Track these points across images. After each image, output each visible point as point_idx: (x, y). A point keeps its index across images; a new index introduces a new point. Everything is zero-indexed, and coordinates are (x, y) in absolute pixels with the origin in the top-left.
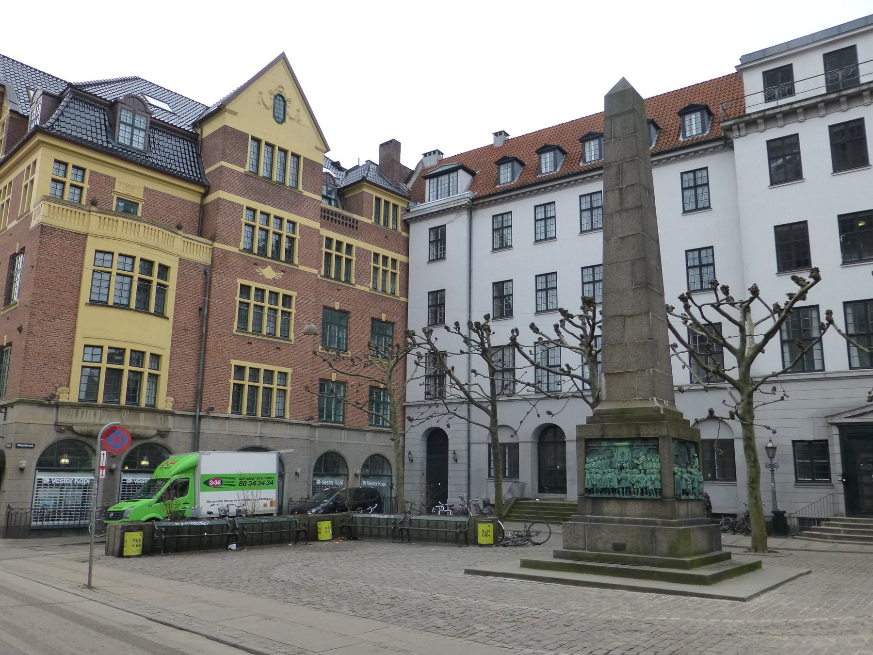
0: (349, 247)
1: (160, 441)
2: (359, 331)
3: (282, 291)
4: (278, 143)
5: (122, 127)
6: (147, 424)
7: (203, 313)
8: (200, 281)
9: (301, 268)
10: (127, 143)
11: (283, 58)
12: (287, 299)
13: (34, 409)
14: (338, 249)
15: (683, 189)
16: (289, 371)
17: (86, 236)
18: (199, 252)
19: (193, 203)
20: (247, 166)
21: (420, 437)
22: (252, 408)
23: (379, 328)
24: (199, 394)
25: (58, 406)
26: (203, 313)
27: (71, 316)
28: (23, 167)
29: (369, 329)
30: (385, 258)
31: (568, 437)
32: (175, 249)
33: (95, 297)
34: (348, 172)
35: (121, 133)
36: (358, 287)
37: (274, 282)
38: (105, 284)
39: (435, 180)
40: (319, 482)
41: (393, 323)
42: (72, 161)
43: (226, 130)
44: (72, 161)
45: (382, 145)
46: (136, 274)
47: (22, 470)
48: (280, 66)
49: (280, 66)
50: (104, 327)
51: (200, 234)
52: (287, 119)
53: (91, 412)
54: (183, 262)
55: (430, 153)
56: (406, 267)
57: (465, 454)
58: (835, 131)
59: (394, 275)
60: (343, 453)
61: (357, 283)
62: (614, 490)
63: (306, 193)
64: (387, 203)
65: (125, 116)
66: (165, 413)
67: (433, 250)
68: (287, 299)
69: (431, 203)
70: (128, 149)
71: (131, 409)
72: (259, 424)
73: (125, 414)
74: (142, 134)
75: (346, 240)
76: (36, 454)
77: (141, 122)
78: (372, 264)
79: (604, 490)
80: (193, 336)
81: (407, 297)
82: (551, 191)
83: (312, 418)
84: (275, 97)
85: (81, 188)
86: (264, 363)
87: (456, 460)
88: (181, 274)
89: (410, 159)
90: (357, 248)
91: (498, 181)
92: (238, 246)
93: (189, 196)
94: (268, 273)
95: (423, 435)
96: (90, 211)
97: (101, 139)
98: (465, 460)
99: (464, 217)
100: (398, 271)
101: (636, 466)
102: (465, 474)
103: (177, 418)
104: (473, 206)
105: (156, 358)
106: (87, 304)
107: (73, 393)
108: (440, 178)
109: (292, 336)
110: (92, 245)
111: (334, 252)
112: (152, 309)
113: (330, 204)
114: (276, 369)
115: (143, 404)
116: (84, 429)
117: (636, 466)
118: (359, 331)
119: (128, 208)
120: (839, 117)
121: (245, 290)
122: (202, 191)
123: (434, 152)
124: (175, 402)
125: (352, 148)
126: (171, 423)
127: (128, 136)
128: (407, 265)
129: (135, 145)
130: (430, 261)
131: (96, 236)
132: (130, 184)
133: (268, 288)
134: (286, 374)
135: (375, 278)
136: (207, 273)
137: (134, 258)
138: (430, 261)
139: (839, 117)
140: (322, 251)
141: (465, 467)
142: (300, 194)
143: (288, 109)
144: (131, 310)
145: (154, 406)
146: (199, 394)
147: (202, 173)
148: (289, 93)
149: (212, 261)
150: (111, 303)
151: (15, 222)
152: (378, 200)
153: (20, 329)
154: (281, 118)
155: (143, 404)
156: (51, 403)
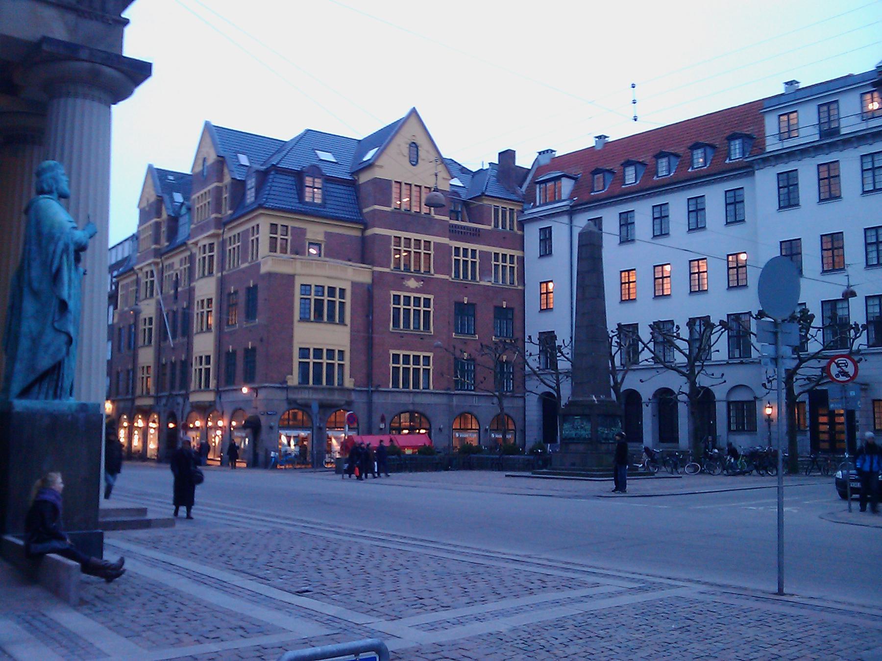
0: (474, 251)
2: (485, 316)
5: (307, 189)
9: (437, 276)
10: (316, 180)
11: (414, 112)
12: (427, 302)
14: (465, 255)
15: (727, 204)
16: (431, 355)
18: (362, 274)
22: (416, 385)
28: (249, 226)
29: (492, 315)
30: (504, 256)
31: (644, 399)
32: (348, 275)
35: (307, 194)
36: (482, 283)
37: (416, 290)
38: (307, 306)
41: (512, 309)
42: (280, 222)
43: (377, 182)
44: (280, 222)
48: (413, 120)
49: (413, 120)
50: (308, 335)
53: (307, 391)
54: (354, 285)
55: (544, 152)
56: (522, 260)
59: (512, 268)
62: (574, 439)
63: (437, 217)
65: (308, 181)
68: (427, 302)
70: (313, 204)
72: (411, 395)
77: (318, 183)
79: (570, 439)
83: (449, 389)
84: (410, 146)
88: (353, 293)
89: (525, 160)
93: (352, 232)
94: (412, 283)
97: (294, 204)
99: (565, 219)
100: (515, 265)
101: (582, 428)
104: (571, 212)
105: (341, 353)
107: (294, 380)
114: (422, 354)
116: (303, 402)
117: (582, 428)
118: (485, 316)
125: (478, 156)
130: (541, 256)
131: (300, 275)
132: (316, 231)
133: (412, 295)
134: (429, 357)
135: (496, 273)
143: (420, 153)
146: (369, 376)
147: (361, 213)
148: (421, 140)
151: (246, 265)
153: (261, 340)
154: (414, 161)
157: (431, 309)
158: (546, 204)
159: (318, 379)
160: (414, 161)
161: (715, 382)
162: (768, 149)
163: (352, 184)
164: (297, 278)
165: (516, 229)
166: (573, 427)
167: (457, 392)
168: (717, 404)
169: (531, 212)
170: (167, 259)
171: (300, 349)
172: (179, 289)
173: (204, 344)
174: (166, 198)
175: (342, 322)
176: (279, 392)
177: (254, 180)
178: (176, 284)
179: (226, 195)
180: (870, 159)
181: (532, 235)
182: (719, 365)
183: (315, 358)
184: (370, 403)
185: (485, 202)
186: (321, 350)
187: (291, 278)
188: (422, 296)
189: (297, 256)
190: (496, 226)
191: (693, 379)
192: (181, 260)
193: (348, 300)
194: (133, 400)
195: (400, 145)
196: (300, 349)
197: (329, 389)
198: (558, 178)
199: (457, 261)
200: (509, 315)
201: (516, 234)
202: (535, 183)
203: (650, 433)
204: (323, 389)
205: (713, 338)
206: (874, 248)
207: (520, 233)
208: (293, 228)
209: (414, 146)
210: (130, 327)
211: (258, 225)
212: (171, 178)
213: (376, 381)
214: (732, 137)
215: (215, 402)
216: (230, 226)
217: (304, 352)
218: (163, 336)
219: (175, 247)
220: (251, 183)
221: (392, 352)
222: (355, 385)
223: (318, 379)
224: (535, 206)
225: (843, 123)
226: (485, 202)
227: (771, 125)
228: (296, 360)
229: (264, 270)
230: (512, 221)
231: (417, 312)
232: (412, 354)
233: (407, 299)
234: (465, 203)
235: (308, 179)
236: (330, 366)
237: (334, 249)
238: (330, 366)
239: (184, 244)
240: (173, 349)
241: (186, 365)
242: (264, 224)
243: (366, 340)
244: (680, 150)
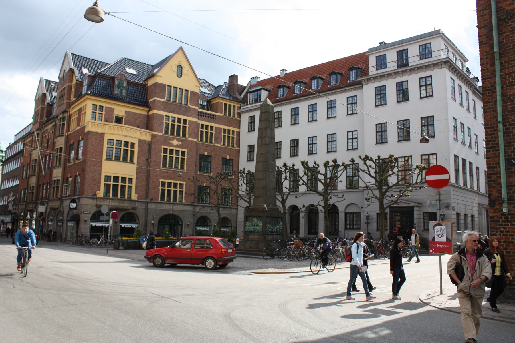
0: (212, 127)
1: (133, 211)
6: (128, 205)
8: (147, 147)
12: (183, 153)
13: (188, 206)
14: (207, 129)
18: (146, 136)
20: (166, 98)
22: (169, 199)
23: (226, 162)
24: (147, 194)
25: (97, 198)
29: (221, 163)
32: (136, 135)
33: (108, 157)
34: (216, 88)
37: (177, 146)
40: (198, 228)
41: (232, 160)
43: (156, 84)
45: (230, 77)
46: (122, 148)
47: (86, 221)
48: (180, 52)
49: (180, 52)
50: (111, 168)
51: (147, 129)
52: (183, 75)
54: (140, 141)
56: (239, 134)
58: (399, 85)
60: (209, 216)
61: (215, 143)
62: (252, 232)
63: (191, 107)
66: (135, 201)
68: (183, 153)
71: (122, 200)
75: (210, 124)
76: (90, 216)
78: (223, 134)
79: (250, 232)
81: (239, 147)
82: (297, 102)
83: (194, 202)
84: (178, 67)
85: (102, 114)
88: (139, 146)
89: (243, 81)
90: (216, 127)
92: (162, 132)
94: (175, 142)
100: (235, 136)
103: (139, 203)
105: (130, 180)
107: (101, 193)
109: (185, 168)
111: (205, 130)
112: (129, 161)
115: (126, 197)
117: (257, 225)
119: (119, 120)
120: (399, 79)
121: (165, 150)
122: (148, 109)
123: (255, 77)
126: (137, 205)
128: (240, 133)
133: (175, 149)
135: (224, 140)
137: (121, 141)
138: (249, 131)
139: (399, 79)
140: (198, 131)
143: (183, 71)
145: (130, 198)
146: (147, 194)
148: (184, 64)
154: (180, 74)
155: (126, 197)
157: (186, 157)
158: (253, 103)
159: (115, 193)
160: (180, 74)
161: (339, 199)
162: (370, 74)
164: (105, 135)
165: (236, 116)
166: (252, 224)
167: (199, 204)
168: (340, 214)
169: (244, 108)
171: (105, 176)
175: (132, 161)
176: (91, 200)
177: (87, 80)
178: (48, 141)
179: (73, 90)
180: (424, 80)
181: (245, 120)
182: (342, 192)
184: (147, 209)
186: (118, 177)
187: (102, 135)
188: (181, 150)
189: (107, 123)
190: (225, 114)
191: (326, 196)
193: (136, 150)
195: (172, 65)
196: (105, 176)
197: (122, 200)
198: (260, 90)
199: (202, 132)
200: (230, 163)
201: (236, 119)
202: (247, 93)
203: (303, 230)
204: (118, 199)
205: (338, 174)
206: (424, 88)
207: (238, 119)
208: (106, 107)
209: (180, 67)
210: (28, 164)
211: (86, 105)
212: (53, 84)
213: (150, 197)
214: (352, 69)
217: (108, 178)
220: (86, 82)
221: (161, 180)
222: (138, 198)
223: (115, 193)
224: (247, 105)
225: (410, 60)
227: (372, 61)
228: (103, 182)
229: (86, 131)
230: (234, 112)
231: (177, 159)
232: (167, 181)
233: (171, 151)
234: (209, 102)
236: (123, 187)
237: (131, 121)
238: (123, 187)
243: (145, 174)
244: (324, 76)
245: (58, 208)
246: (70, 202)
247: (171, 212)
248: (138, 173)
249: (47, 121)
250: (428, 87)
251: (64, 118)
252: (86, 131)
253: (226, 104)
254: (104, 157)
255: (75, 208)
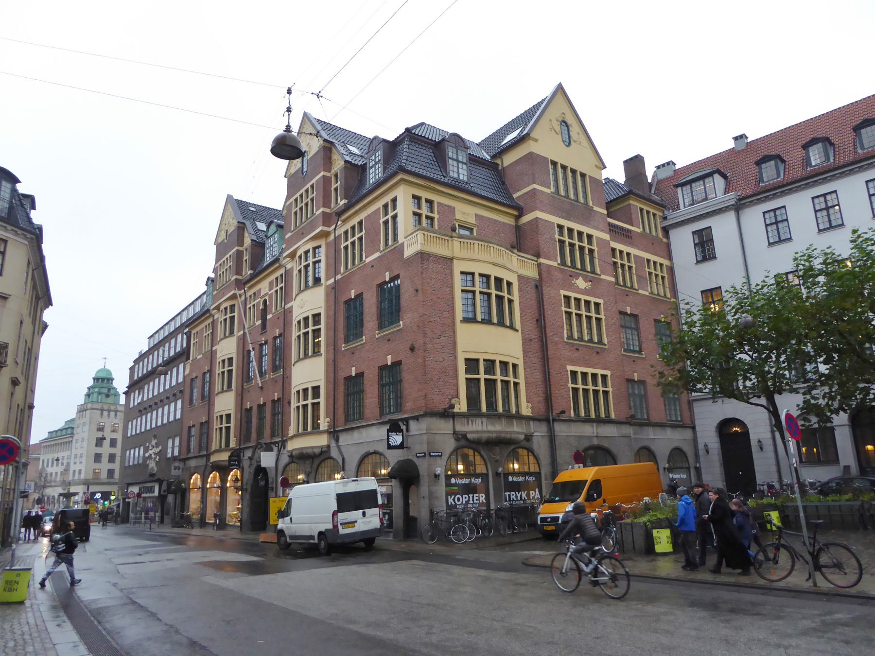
3: (593, 300)
4: (570, 165)
7: (541, 322)
8: (532, 294)
10: (456, 176)
11: (560, 89)
12: (597, 305)
17: (451, 259)
19: (510, 225)
21: (714, 429)
24: (548, 399)
26: (541, 322)
27: (451, 333)
28: (379, 204)
32: (515, 268)
37: (585, 292)
39: (688, 187)
42: (424, 195)
48: (559, 96)
49: (559, 96)
54: (520, 278)
55: (663, 165)
56: (671, 270)
57: (771, 442)
63: (595, 208)
64: (648, 212)
67: (699, 250)
69: (685, 210)
70: (457, 180)
73: (504, 421)
74: (465, 167)
80: (536, 345)
86: (590, 367)
87: (761, 448)
91: (761, 180)
94: (581, 283)
95: (717, 427)
96: (452, 237)
98: (772, 448)
99: (731, 216)
102: (773, 461)
104: (738, 207)
106: (461, 321)
107: (462, 406)
108: (693, 185)
109: (605, 341)
110: (458, 267)
113: (319, 261)
115: (484, 409)
122: (516, 213)
123: (668, 163)
124: (532, 408)
127: (455, 169)
129: (461, 177)
130: (698, 262)
132: (466, 212)
136: (538, 287)
138: (698, 262)
141: (772, 455)
142: (591, 209)
144: (494, 324)
146: (548, 399)
147: (511, 197)
148: (570, 120)
149: (540, 274)
150: (479, 319)
151: (377, 255)
152: (641, 210)
153: (412, 349)
156: (447, 414)
163: (491, 166)
170: (250, 288)
171: (466, 359)
172: (269, 317)
173: (309, 372)
174: (248, 224)
181: (683, 242)
183: (486, 373)
185: (631, 202)
186: (477, 361)
192: (271, 283)
194: (208, 456)
196: (466, 359)
211: (394, 200)
213: (557, 410)
215: (329, 446)
216: (343, 217)
217: (472, 364)
218: (246, 377)
219: (259, 269)
226: (631, 202)
228: (462, 376)
229: (408, 252)
235: (450, 149)
239: (277, 260)
240: (261, 388)
241: (280, 405)
242: (403, 195)
243: (540, 344)
245: (322, 452)
246: (388, 431)
247: (595, 442)
248: (525, 352)
249: (252, 277)
250: (780, 225)
251: (232, 307)
252: (408, 252)
253: (641, 210)
254: (459, 315)
255: (401, 446)
